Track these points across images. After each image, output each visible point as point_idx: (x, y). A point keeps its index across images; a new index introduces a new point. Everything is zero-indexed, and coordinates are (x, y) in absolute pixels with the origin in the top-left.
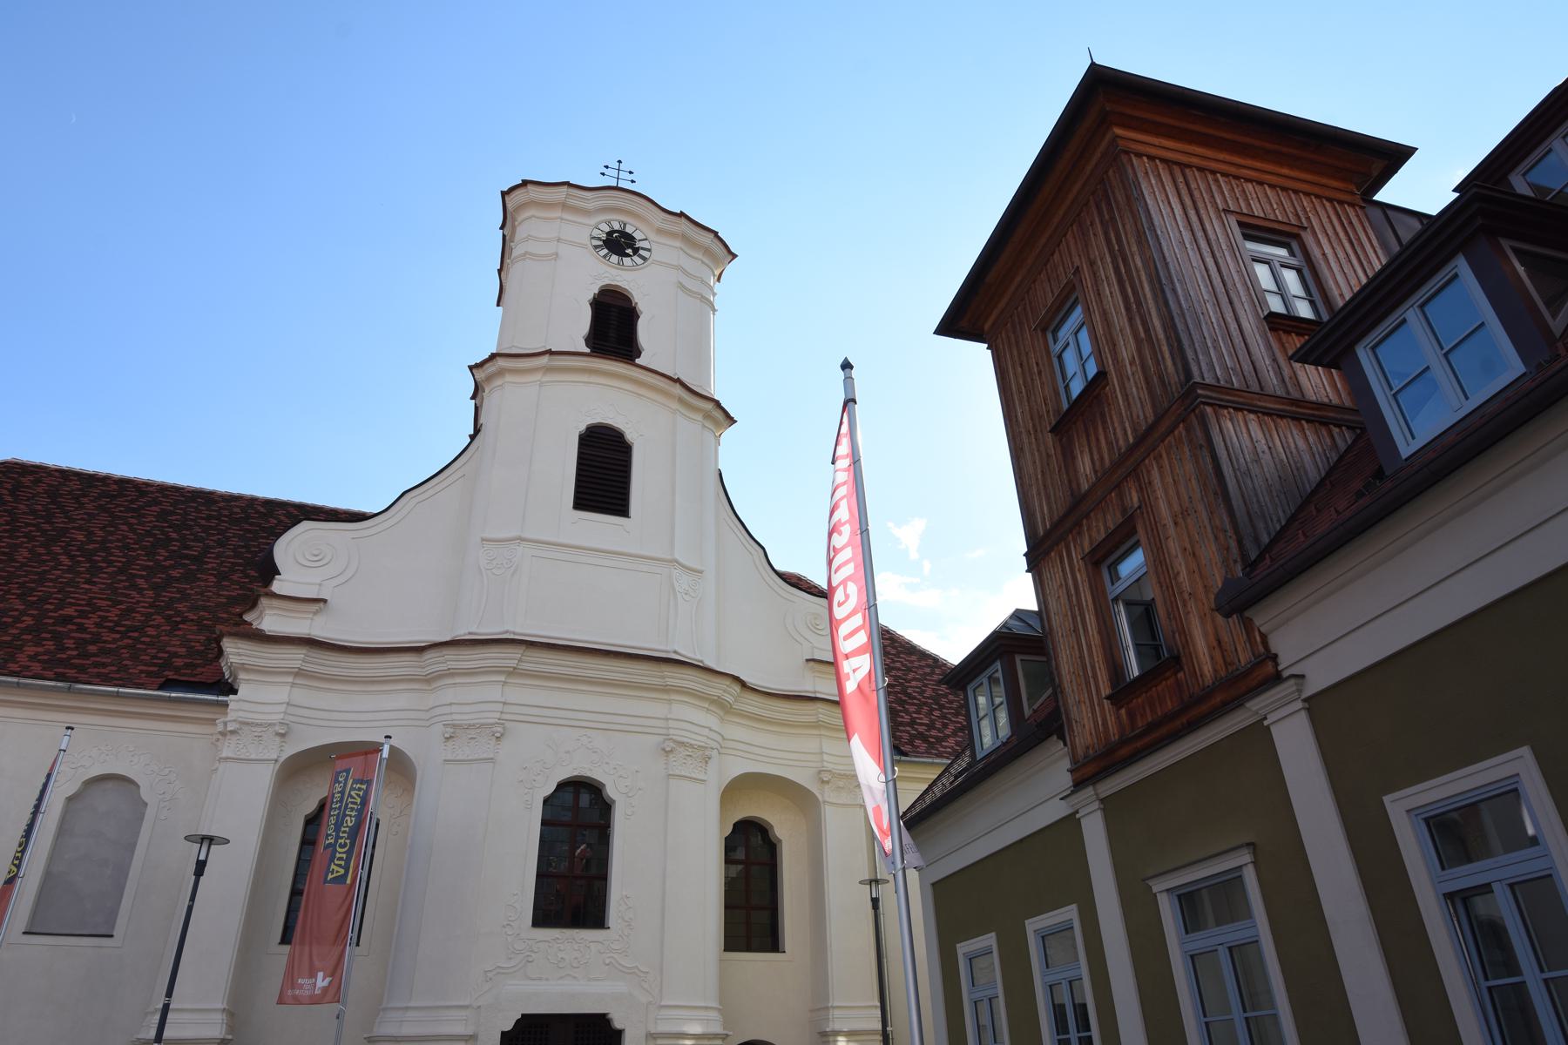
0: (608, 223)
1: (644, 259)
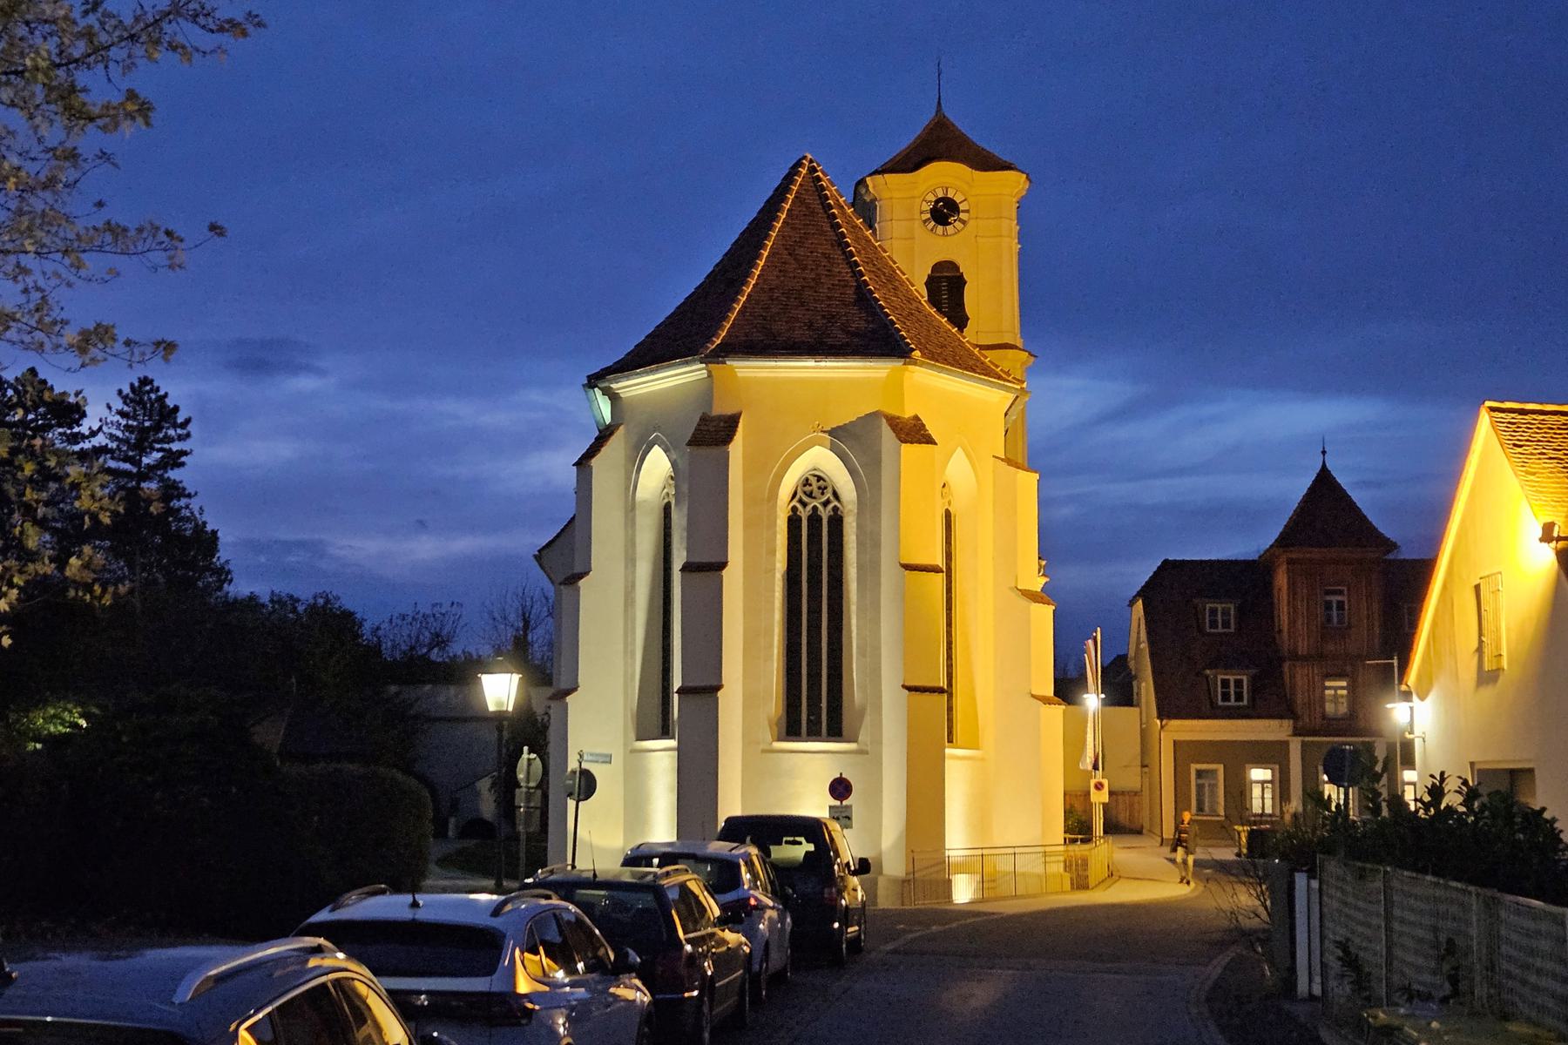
1: (964, 222)
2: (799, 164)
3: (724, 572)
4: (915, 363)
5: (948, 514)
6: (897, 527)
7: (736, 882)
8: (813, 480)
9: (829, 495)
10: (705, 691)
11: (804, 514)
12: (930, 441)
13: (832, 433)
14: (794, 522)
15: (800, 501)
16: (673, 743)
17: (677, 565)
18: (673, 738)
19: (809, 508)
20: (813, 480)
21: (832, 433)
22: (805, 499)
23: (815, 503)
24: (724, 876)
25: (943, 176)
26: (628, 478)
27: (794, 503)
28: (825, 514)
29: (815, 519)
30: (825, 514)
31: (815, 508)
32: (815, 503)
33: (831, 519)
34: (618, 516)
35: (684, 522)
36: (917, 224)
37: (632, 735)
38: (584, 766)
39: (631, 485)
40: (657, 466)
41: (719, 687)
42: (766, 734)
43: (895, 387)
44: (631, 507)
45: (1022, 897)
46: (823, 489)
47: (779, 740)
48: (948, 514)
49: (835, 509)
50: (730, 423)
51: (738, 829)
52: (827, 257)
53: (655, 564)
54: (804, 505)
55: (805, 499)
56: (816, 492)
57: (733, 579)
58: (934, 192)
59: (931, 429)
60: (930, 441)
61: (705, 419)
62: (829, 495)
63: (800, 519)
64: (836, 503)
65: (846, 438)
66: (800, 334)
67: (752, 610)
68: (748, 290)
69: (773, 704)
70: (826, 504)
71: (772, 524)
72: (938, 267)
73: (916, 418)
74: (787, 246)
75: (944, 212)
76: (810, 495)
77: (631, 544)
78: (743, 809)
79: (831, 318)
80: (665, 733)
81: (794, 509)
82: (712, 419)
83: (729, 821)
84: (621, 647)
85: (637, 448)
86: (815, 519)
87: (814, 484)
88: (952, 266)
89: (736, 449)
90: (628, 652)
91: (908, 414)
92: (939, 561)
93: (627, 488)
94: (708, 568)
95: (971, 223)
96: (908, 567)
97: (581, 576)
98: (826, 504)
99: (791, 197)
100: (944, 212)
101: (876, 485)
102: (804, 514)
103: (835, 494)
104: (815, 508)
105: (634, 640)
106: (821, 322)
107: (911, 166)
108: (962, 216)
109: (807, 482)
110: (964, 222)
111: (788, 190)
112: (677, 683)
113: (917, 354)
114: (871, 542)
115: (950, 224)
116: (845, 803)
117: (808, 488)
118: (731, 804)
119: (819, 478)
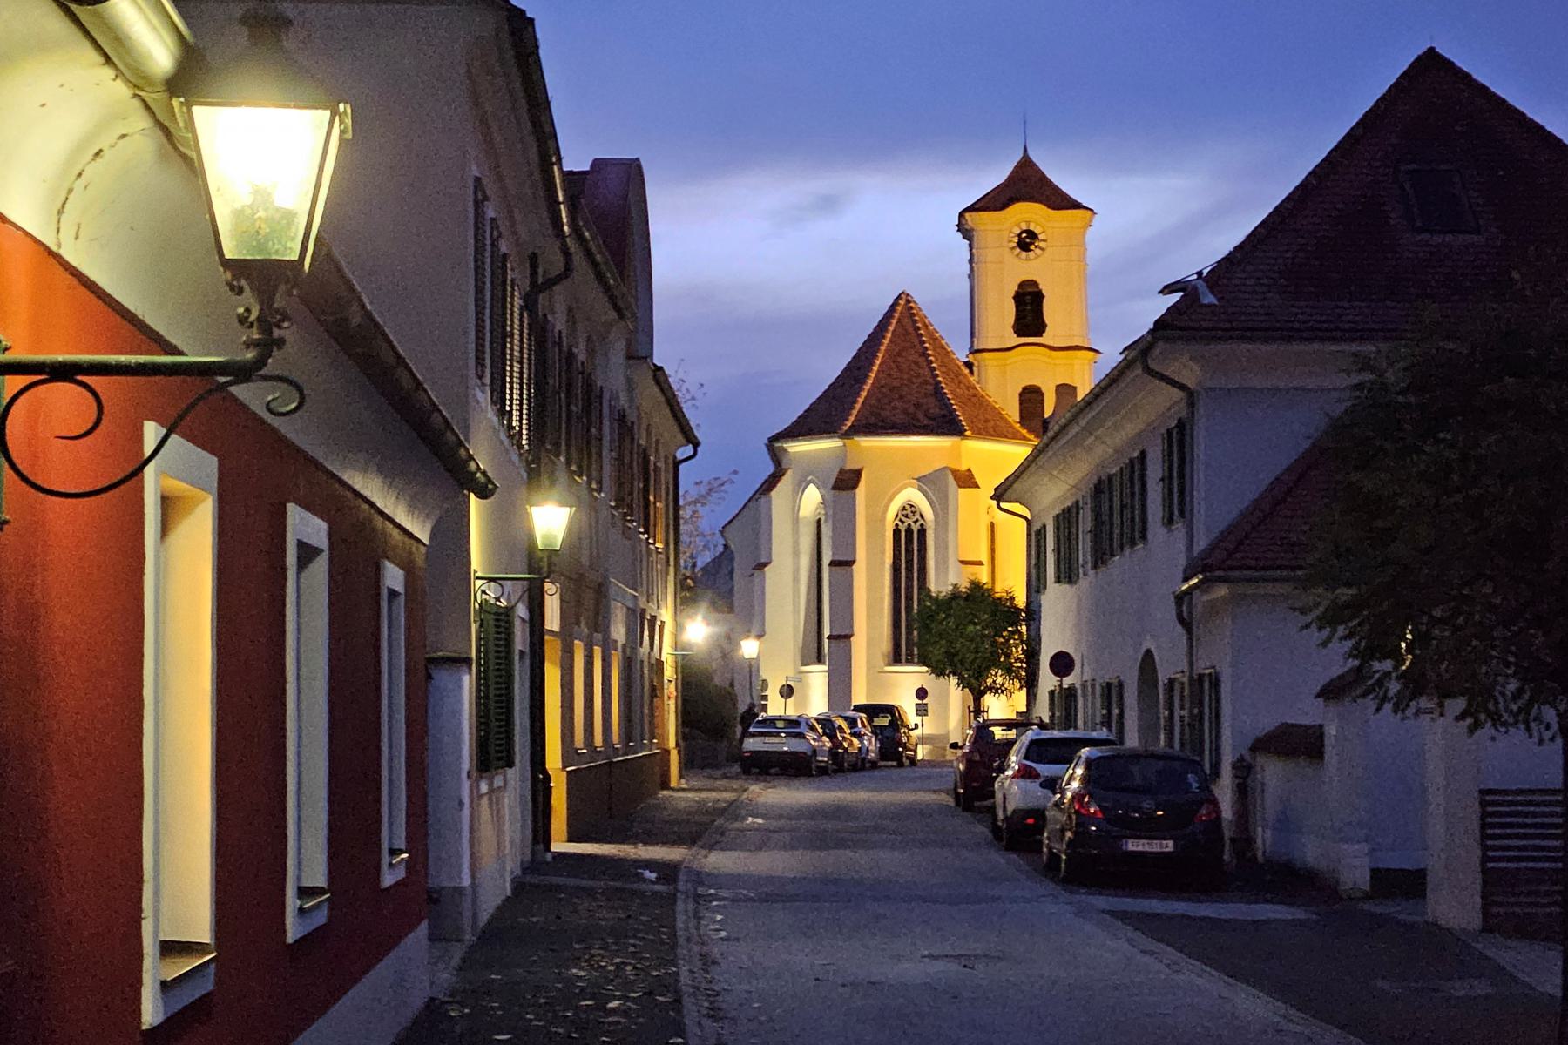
0: (1018, 225)
1: (1042, 249)
2: (899, 297)
3: (854, 567)
4: (966, 437)
5: (992, 525)
6: (956, 538)
7: (856, 726)
8: (908, 507)
9: (917, 516)
10: (843, 638)
11: (903, 528)
12: (977, 486)
13: (918, 479)
14: (896, 532)
15: (900, 520)
16: (825, 668)
17: (826, 561)
18: (824, 664)
19: (906, 524)
20: (908, 507)
21: (918, 479)
22: (903, 519)
23: (910, 521)
24: (852, 722)
25: (1027, 214)
26: (794, 502)
27: (897, 521)
28: (915, 528)
29: (909, 531)
30: (915, 528)
31: (909, 525)
32: (910, 521)
33: (919, 531)
34: (788, 526)
35: (830, 533)
36: (1007, 250)
37: (799, 662)
38: (789, 683)
39: (795, 510)
40: (812, 498)
41: (852, 635)
42: (880, 662)
43: (956, 453)
44: (796, 520)
45: (652, 701)
46: (913, 513)
47: (889, 665)
48: (992, 525)
49: (922, 525)
50: (857, 474)
51: (858, 708)
52: (916, 363)
53: (812, 555)
54: (903, 522)
55: (903, 519)
56: (910, 515)
57: (860, 571)
58: (1018, 225)
59: (978, 479)
60: (977, 486)
61: (842, 471)
62: (917, 516)
63: (900, 531)
64: (922, 522)
65: (928, 482)
66: (899, 418)
67: (872, 587)
68: (867, 387)
69: (885, 644)
70: (915, 522)
71: (883, 536)
72: (1022, 285)
73: (969, 470)
74: (894, 357)
75: (1027, 241)
76: (906, 516)
77: (796, 543)
78: (869, 694)
79: (918, 406)
80: (820, 660)
81: (897, 525)
82: (846, 472)
83: (855, 706)
84: (790, 608)
85: (799, 485)
86: (909, 531)
87: (909, 510)
88: (1034, 283)
89: (861, 492)
90: (796, 611)
91: (964, 468)
92: (985, 557)
93: (793, 510)
94: (844, 564)
95: (1049, 250)
96: (962, 562)
97: (766, 564)
98: (915, 522)
99: (894, 322)
100: (1027, 241)
101: (945, 509)
102: (903, 528)
103: (922, 516)
104: (909, 525)
105: (799, 603)
106: (912, 409)
107: (998, 205)
108: (1042, 244)
109: (904, 509)
110: (1042, 249)
111: (892, 317)
112: (826, 632)
113: (968, 433)
114: (942, 547)
115: (1031, 250)
116: (924, 701)
117: (905, 512)
118: (860, 697)
119: (912, 506)
